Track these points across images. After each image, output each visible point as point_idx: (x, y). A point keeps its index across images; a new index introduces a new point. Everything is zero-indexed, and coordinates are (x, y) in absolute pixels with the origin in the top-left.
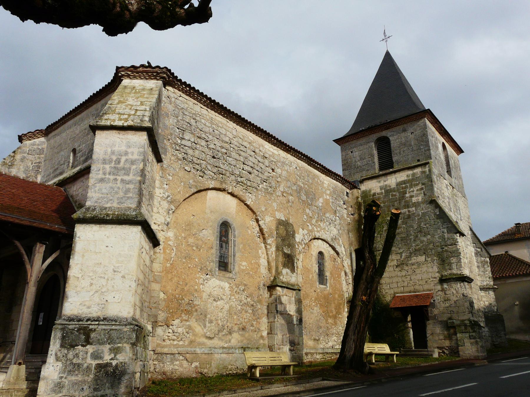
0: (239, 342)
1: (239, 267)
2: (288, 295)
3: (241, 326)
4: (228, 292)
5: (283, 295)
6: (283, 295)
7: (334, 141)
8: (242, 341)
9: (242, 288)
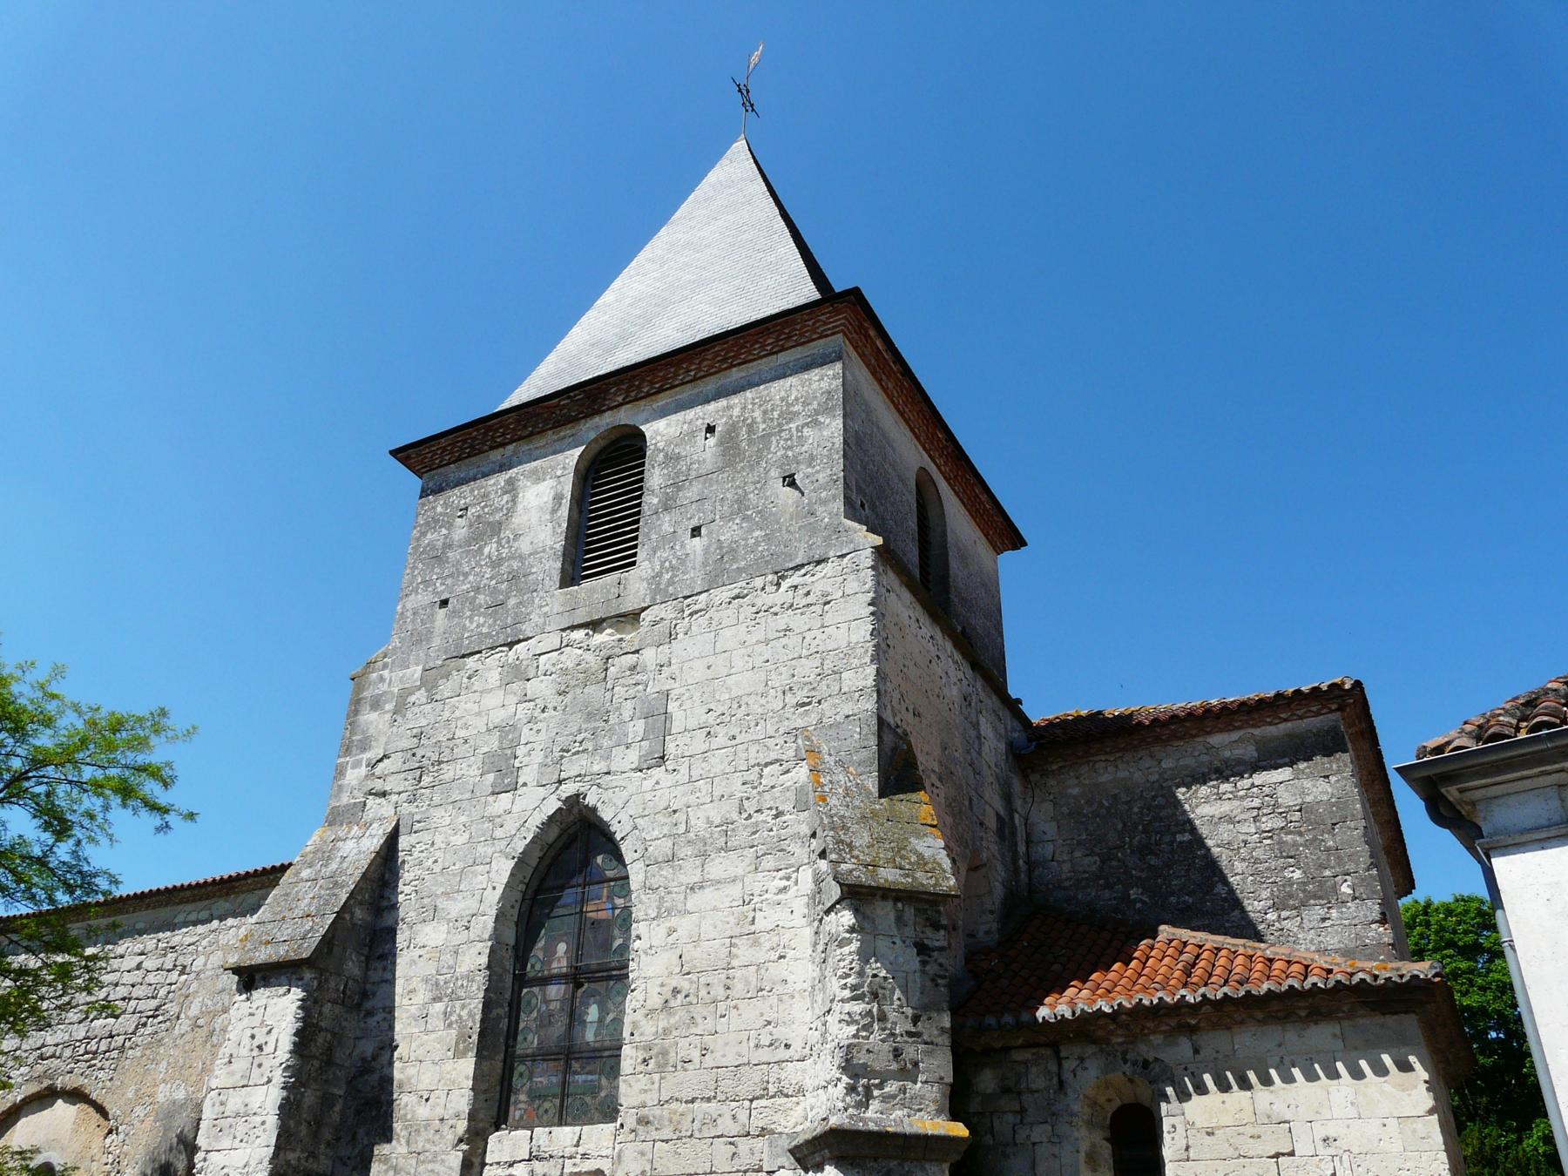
7: (395, 453)
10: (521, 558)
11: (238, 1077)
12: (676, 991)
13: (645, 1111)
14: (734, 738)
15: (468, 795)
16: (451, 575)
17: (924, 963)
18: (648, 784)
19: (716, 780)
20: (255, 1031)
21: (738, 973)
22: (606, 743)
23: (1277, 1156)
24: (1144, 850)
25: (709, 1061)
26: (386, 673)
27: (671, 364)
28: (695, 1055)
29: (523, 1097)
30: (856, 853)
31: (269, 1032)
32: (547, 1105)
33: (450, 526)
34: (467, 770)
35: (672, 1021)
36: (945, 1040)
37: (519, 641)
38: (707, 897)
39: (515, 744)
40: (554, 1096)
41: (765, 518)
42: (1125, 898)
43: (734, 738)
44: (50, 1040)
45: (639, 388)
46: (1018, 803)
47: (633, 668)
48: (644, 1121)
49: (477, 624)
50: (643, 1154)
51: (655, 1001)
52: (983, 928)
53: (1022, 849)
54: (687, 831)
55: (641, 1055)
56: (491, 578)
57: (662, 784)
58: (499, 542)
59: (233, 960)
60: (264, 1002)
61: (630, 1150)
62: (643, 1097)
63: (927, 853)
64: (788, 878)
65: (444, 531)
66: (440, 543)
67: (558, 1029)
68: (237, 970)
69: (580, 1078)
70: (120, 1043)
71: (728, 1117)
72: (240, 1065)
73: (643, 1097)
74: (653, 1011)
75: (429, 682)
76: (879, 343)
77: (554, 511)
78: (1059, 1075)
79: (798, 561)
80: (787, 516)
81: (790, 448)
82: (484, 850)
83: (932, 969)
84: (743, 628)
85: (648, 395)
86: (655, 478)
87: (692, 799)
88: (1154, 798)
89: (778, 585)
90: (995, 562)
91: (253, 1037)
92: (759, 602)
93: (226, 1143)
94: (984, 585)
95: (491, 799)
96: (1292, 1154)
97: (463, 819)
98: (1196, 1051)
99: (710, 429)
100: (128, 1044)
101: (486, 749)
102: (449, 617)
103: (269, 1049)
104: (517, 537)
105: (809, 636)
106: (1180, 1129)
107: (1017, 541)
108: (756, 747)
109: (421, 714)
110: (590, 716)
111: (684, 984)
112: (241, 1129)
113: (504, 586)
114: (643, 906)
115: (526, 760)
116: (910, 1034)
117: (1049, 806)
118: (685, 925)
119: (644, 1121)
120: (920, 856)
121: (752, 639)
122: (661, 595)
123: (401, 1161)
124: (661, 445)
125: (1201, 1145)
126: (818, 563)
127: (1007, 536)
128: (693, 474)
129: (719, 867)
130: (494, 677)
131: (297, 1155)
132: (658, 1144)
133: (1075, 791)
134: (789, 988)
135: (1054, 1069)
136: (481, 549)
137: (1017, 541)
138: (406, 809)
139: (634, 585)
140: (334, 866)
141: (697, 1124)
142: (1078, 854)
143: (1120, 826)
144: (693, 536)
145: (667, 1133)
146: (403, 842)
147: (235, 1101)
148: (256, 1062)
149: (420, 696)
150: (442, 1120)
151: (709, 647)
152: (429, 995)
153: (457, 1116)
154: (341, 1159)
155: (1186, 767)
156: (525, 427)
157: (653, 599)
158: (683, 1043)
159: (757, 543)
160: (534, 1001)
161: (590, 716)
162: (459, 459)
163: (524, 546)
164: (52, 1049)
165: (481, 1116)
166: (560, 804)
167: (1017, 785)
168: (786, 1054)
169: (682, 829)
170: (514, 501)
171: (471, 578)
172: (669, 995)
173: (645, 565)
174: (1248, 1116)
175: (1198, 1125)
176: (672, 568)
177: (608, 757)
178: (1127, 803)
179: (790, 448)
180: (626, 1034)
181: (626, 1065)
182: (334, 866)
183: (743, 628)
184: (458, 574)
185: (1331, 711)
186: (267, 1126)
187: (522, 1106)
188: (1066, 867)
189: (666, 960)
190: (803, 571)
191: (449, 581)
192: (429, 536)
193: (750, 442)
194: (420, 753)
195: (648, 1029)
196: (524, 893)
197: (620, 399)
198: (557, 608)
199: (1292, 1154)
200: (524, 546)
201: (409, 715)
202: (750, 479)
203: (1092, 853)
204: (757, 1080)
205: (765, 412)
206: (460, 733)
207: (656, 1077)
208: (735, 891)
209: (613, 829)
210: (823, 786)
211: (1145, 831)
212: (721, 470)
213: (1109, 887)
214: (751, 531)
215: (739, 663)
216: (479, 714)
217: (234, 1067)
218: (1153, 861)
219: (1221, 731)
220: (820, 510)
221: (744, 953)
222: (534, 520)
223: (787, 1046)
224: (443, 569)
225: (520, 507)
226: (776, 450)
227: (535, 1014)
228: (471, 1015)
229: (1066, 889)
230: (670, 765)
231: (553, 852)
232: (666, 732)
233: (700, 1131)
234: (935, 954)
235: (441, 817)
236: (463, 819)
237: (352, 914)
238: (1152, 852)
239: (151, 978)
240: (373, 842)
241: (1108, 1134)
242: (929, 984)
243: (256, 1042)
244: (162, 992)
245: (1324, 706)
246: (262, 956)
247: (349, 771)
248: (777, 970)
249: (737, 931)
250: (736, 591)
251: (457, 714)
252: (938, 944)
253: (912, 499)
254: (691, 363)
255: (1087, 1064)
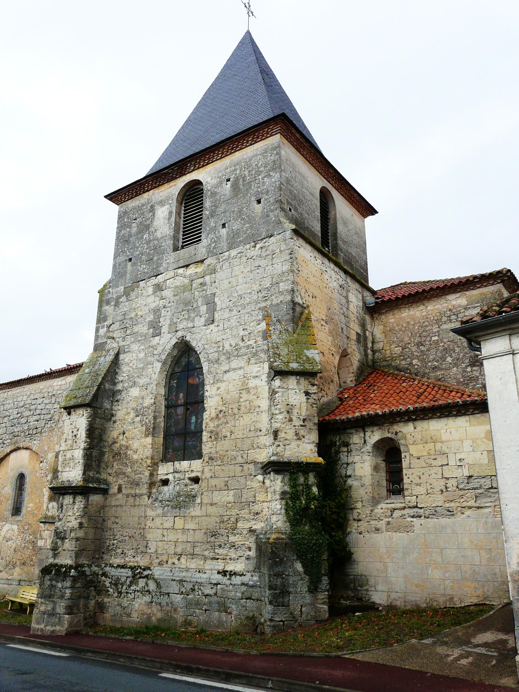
0: (19, 575)
1: (26, 509)
2: (49, 529)
3: (22, 561)
4: (17, 533)
5: (44, 531)
6: (44, 531)
7: (106, 197)
8: (21, 575)
9: (26, 527)
10: (158, 239)
11: (69, 446)
12: (221, 411)
13: (211, 455)
14: (240, 311)
15: (143, 338)
16: (132, 248)
17: (308, 399)
18: (208, 331)
19: (233, 329)
20: (73, 430)
21: (243, 404)
22: (192, 315)
23: (442, 466)
24: (420, 344)
25: (233, 437)
26: (110, 290)
27: (211, 152)
28: (228, 434)
29: (170, 450)
30: (281, 358)
31: (78, 430)
32: (179, 453)
33: (130, 227)
34: (143, 329)
35: (220, 422)
36: (316, 427)
37: (159, 275)
38: (231, 375)
39: (159, 317)
40: (181, 450)
41: (251, 219)
42: (411, 364)
43: (240, 311)
44: (16, 430)
45: (199, 163)
46: (369, 327)
47: (201, 284)
48: (211, 458)
49: (143, 268)
50: (211, 470)
51: (213, 415)
52: (349, 380)
53: (370, 345)
54: (223, 349)
55: (209, 435)
56: (147, 249)
57: (214, 331)
58: (149, 233)
59: (63, 404)
60: (75, 419)
61: (207, 469)
62: (210, 450)
63: (310, 356)
64: (260, 367)
65: (128, 229)
66: (127, 235)
67: (181, 426)
68: (65, 408)
69: (190, 443)
70: (40, 431)
71: (240, 456)
72: (70, 442)
73: (210, 450)
74: (212, 419)
75: (127, 293)
76: (298, 135)
77: (169, 219)
78: (364, 438)
79: (263, 237)
80: (258, 218)
81: (259, 187)
82: (150, 359)
83: (311, 401)
84: (242, 266)
85: (203, 166)
86: (207, 203)
87: (225, 337)
88: (424, 322)
89: (255, 247)
90: (364, 222)
91: (73, 432)
92: (248, 255)
93: (67, 469)
94: (356, 233)
95: (152, 339)
96: (448, 465)
97: (142, 347)
98: (415, 428)
99: (228, 180)
100: (43, 431)
101: (149, 319)
102: (132, 266)
103: (78, 436)
104: (156, 230)
105: (267, 268)
106: (408, 457)
107: (372, 211)
108: (248, 315)
109: (124, 307)
110: (186, 304)
111: (224, 409)
112: (72, 464)
113: (152, 252)
114: (208, 379)
115: (164, 323)
116: (301, 426)
117: (381, 327)
118: (223, 386)
119: (211, 458)
120: (308, 358)
121: (246, 271)
122: (211, 253)
123: (129, 474)
124: (209, 188)
125: (415, 462)
126: (270, 237)
127: (366, 209)
128: (222, 200)
129: (235, 363)
130: (150, 290)
131: (92, 473)
132: (216, 467)
133: (392, 321)
134: (261, 409)
135: (363, 435)
136: (142, 236)
137: (372, 211)
138: (122, 344)
139: (200, 249)
140: (96, 367)
141: (229, 459)
142: (393, 346)
143: (410, 334)
144: (223, 228)
145: (219, 463)
146: (121, 357)
147: (69, 455)
148: (75, 441)
149: (123, 299)
150: (142, 459)
151: (230, 275)
152: (135, 415)
153: (147, 458)
154: (109, 474)
155: (438, 309)
156: (156, 183)
157: (208, 255)
158: (224, 430)
159: (247, 230)
160: (173, 415)
161: (186, 304)
162: (132, 198)
163: (159, 235)
164: (17, 433)
165: (156, 458)
166: (176, 340)
167: (368, 318)
168: (260, 434)
169: (221, 349)
170: (154, 215)
171: (139, 249)
172: (218, 413)
173: (205, 242)
174: (432, 452)
175: (414, 455)
176: (215, 242)
177: (193, 321)
178: (413, 325)
179: (259, 187)
180: (204, 427)
181: (204, 439)
182: (96, 367)
183: (242, 266)
184: (135, 247)
185: (498, 283)
186: (80, 463)
187: (171, 454)
188: (388, 352)
189: (217, 399)
190: (265, 240)
191: (131, 251)
192: (123, 232)
193: (243, 185)
194: (125, 321)
195: (211, 425)
196: (167, 375)
197: (192, 168)
198: (172, 260)
199: (448, 465)
200: (159, 235)
201: (120, 307)
202: (244, 201)
203: (399, 346)
204: (250, 443)
205: (249, 172)
206: (140, 313)
207: (215, 443)
208: (241, 372)
209: (196, 349)
210: (270, 331)
211: (420, 336)
212: (232, 198)
213: (405, 359)
214: (244, 225)
215: (241, 281)
216: (145, 305)
217: (67, 443)
218: (422, 348)
219: (453, 293)
220: (271, 214)
221: (245, 396)
222: (162, 223)
223: (260, 431)
224: (129, 246)
225: (156, 218)
226: (254, 189)
227: (173, 420)
228: (149, 421)
229: (387, 361)
230: (216, 324)
231: (176, 358)
232: (215, 310)
233: (231, 462)
234: (312, 395)
235: (135, 347)
236: (142, 347)
237: (105, 386)
238: (422, 345)
239: (48, 407)
240: (110, 358)
241: (384, 458)
242: (310, 407)
243: (74, 434)
244: (52, 412)
245: (495, 281)
246: (72, 403)
247: (100, 330)
248: (257, 403)
249: (242, 388)
250: (239, 250)
251: (138, 305)
252: (313, 392)
253: (317, 202)
254: (219, 151)
255: (374, 433)
